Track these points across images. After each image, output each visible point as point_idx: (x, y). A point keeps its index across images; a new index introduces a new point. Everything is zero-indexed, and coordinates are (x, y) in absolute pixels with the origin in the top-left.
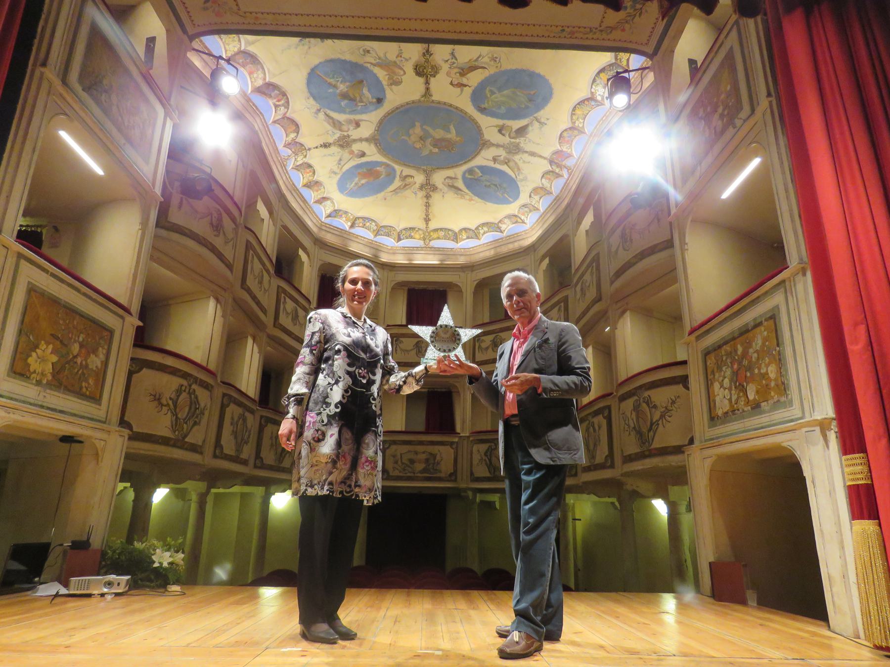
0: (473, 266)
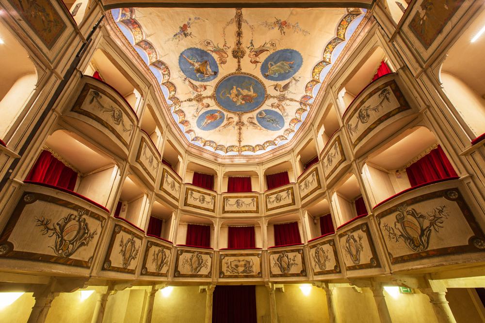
0: (263, 163)
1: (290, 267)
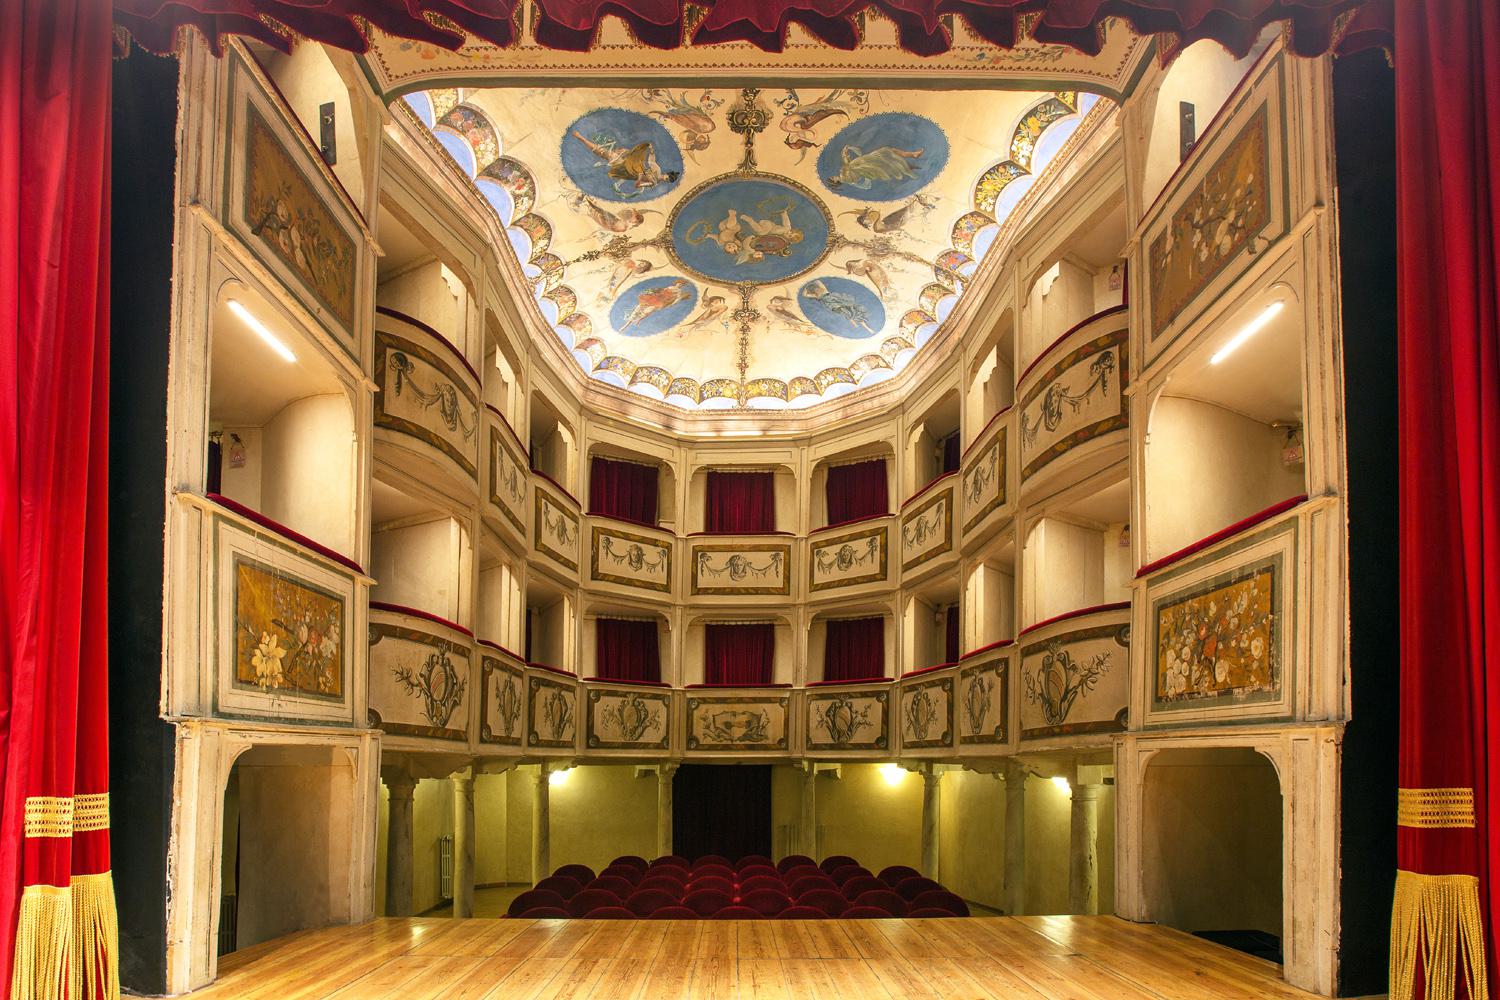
1: (854, 729)
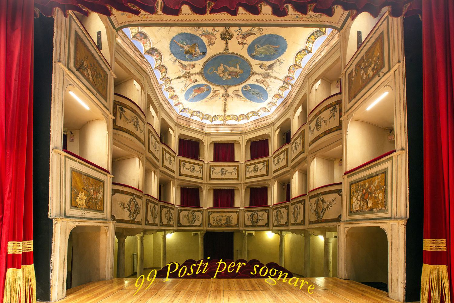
1: (258, 221)
